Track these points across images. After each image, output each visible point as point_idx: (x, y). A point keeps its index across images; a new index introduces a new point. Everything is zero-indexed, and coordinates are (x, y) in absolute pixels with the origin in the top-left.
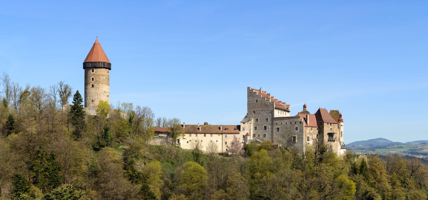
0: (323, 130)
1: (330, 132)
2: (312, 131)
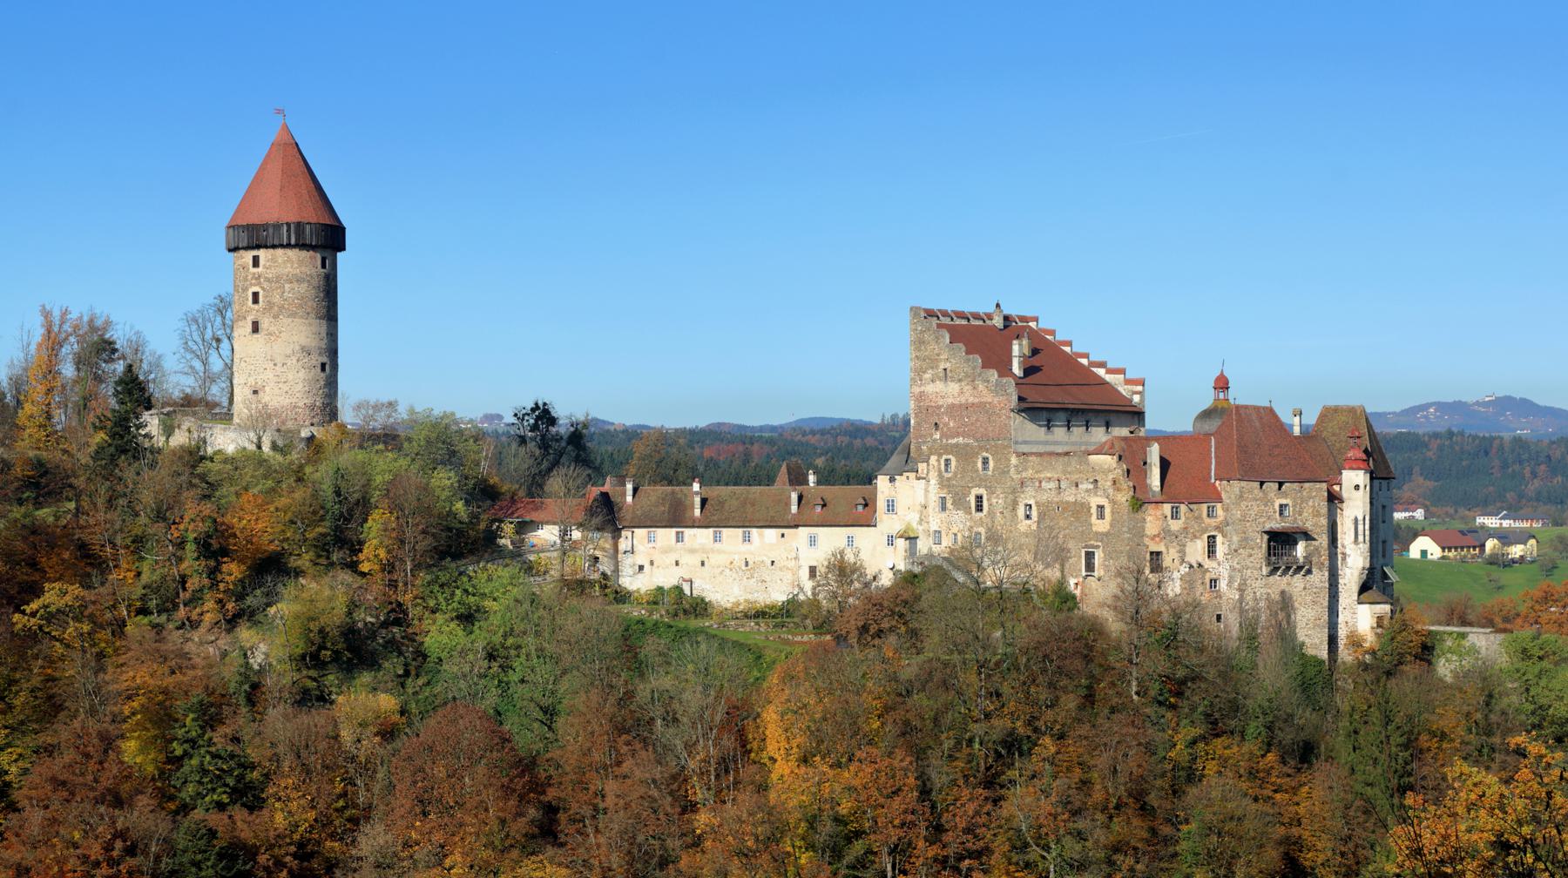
1: (1276, 524)
2: (1175, 526)
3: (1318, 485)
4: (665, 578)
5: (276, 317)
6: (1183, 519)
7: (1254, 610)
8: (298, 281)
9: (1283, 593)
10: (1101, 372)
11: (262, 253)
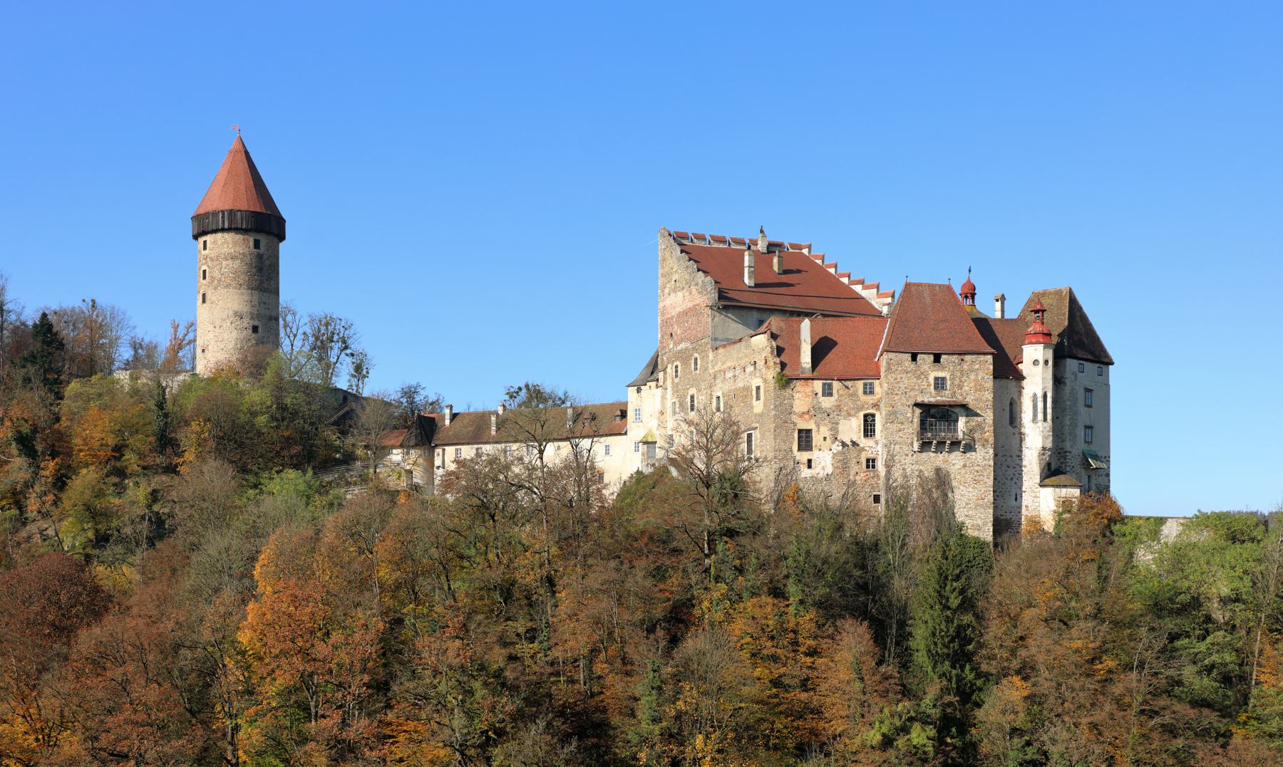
1: (930, 397)
2: (827, 403)
3: (982, 358)
4: (1192, 711)
5: (216, 288)
6: (835, 395)
7: (902, 487)
8: (232, 258)
9: (938, 470)
10: (858, 288)
11: (208, 238)
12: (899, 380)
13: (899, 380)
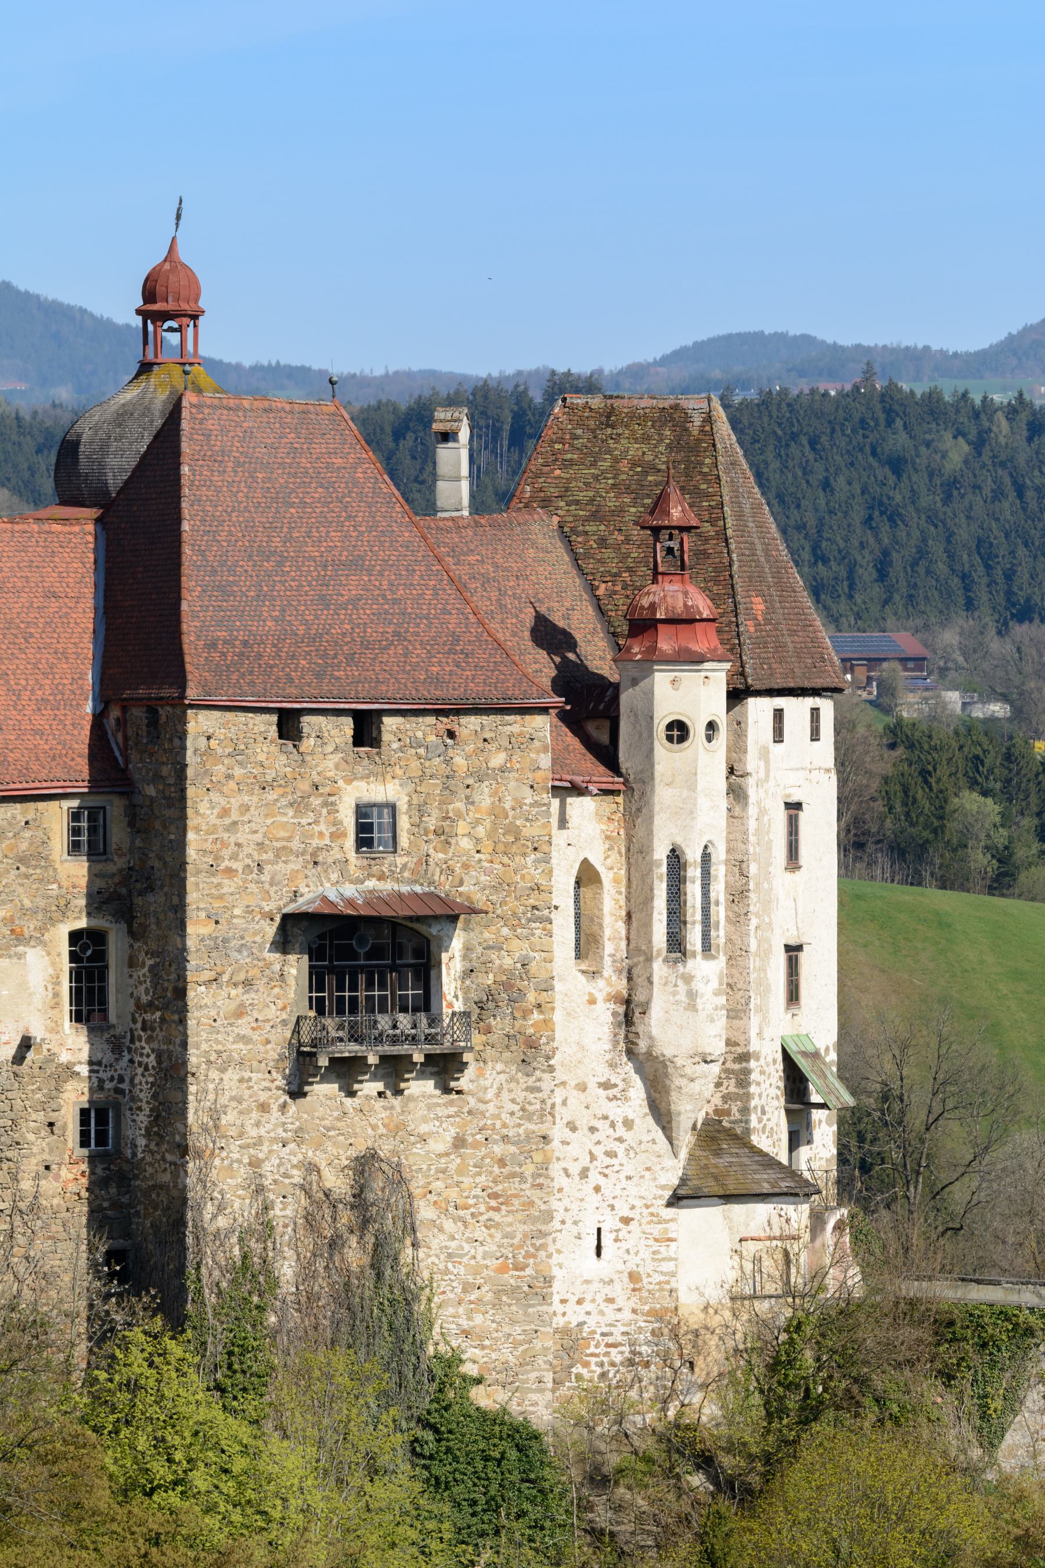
0: (183, 865)
3: (515, 724)
12: (235, 816)
13: (235, 816)
